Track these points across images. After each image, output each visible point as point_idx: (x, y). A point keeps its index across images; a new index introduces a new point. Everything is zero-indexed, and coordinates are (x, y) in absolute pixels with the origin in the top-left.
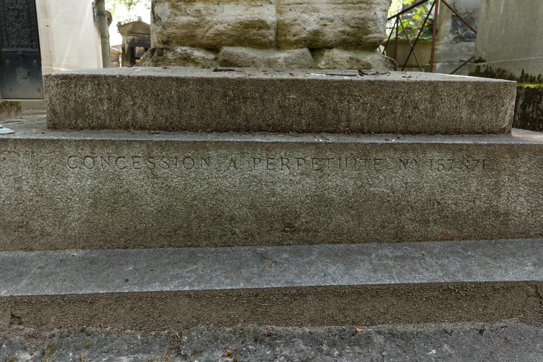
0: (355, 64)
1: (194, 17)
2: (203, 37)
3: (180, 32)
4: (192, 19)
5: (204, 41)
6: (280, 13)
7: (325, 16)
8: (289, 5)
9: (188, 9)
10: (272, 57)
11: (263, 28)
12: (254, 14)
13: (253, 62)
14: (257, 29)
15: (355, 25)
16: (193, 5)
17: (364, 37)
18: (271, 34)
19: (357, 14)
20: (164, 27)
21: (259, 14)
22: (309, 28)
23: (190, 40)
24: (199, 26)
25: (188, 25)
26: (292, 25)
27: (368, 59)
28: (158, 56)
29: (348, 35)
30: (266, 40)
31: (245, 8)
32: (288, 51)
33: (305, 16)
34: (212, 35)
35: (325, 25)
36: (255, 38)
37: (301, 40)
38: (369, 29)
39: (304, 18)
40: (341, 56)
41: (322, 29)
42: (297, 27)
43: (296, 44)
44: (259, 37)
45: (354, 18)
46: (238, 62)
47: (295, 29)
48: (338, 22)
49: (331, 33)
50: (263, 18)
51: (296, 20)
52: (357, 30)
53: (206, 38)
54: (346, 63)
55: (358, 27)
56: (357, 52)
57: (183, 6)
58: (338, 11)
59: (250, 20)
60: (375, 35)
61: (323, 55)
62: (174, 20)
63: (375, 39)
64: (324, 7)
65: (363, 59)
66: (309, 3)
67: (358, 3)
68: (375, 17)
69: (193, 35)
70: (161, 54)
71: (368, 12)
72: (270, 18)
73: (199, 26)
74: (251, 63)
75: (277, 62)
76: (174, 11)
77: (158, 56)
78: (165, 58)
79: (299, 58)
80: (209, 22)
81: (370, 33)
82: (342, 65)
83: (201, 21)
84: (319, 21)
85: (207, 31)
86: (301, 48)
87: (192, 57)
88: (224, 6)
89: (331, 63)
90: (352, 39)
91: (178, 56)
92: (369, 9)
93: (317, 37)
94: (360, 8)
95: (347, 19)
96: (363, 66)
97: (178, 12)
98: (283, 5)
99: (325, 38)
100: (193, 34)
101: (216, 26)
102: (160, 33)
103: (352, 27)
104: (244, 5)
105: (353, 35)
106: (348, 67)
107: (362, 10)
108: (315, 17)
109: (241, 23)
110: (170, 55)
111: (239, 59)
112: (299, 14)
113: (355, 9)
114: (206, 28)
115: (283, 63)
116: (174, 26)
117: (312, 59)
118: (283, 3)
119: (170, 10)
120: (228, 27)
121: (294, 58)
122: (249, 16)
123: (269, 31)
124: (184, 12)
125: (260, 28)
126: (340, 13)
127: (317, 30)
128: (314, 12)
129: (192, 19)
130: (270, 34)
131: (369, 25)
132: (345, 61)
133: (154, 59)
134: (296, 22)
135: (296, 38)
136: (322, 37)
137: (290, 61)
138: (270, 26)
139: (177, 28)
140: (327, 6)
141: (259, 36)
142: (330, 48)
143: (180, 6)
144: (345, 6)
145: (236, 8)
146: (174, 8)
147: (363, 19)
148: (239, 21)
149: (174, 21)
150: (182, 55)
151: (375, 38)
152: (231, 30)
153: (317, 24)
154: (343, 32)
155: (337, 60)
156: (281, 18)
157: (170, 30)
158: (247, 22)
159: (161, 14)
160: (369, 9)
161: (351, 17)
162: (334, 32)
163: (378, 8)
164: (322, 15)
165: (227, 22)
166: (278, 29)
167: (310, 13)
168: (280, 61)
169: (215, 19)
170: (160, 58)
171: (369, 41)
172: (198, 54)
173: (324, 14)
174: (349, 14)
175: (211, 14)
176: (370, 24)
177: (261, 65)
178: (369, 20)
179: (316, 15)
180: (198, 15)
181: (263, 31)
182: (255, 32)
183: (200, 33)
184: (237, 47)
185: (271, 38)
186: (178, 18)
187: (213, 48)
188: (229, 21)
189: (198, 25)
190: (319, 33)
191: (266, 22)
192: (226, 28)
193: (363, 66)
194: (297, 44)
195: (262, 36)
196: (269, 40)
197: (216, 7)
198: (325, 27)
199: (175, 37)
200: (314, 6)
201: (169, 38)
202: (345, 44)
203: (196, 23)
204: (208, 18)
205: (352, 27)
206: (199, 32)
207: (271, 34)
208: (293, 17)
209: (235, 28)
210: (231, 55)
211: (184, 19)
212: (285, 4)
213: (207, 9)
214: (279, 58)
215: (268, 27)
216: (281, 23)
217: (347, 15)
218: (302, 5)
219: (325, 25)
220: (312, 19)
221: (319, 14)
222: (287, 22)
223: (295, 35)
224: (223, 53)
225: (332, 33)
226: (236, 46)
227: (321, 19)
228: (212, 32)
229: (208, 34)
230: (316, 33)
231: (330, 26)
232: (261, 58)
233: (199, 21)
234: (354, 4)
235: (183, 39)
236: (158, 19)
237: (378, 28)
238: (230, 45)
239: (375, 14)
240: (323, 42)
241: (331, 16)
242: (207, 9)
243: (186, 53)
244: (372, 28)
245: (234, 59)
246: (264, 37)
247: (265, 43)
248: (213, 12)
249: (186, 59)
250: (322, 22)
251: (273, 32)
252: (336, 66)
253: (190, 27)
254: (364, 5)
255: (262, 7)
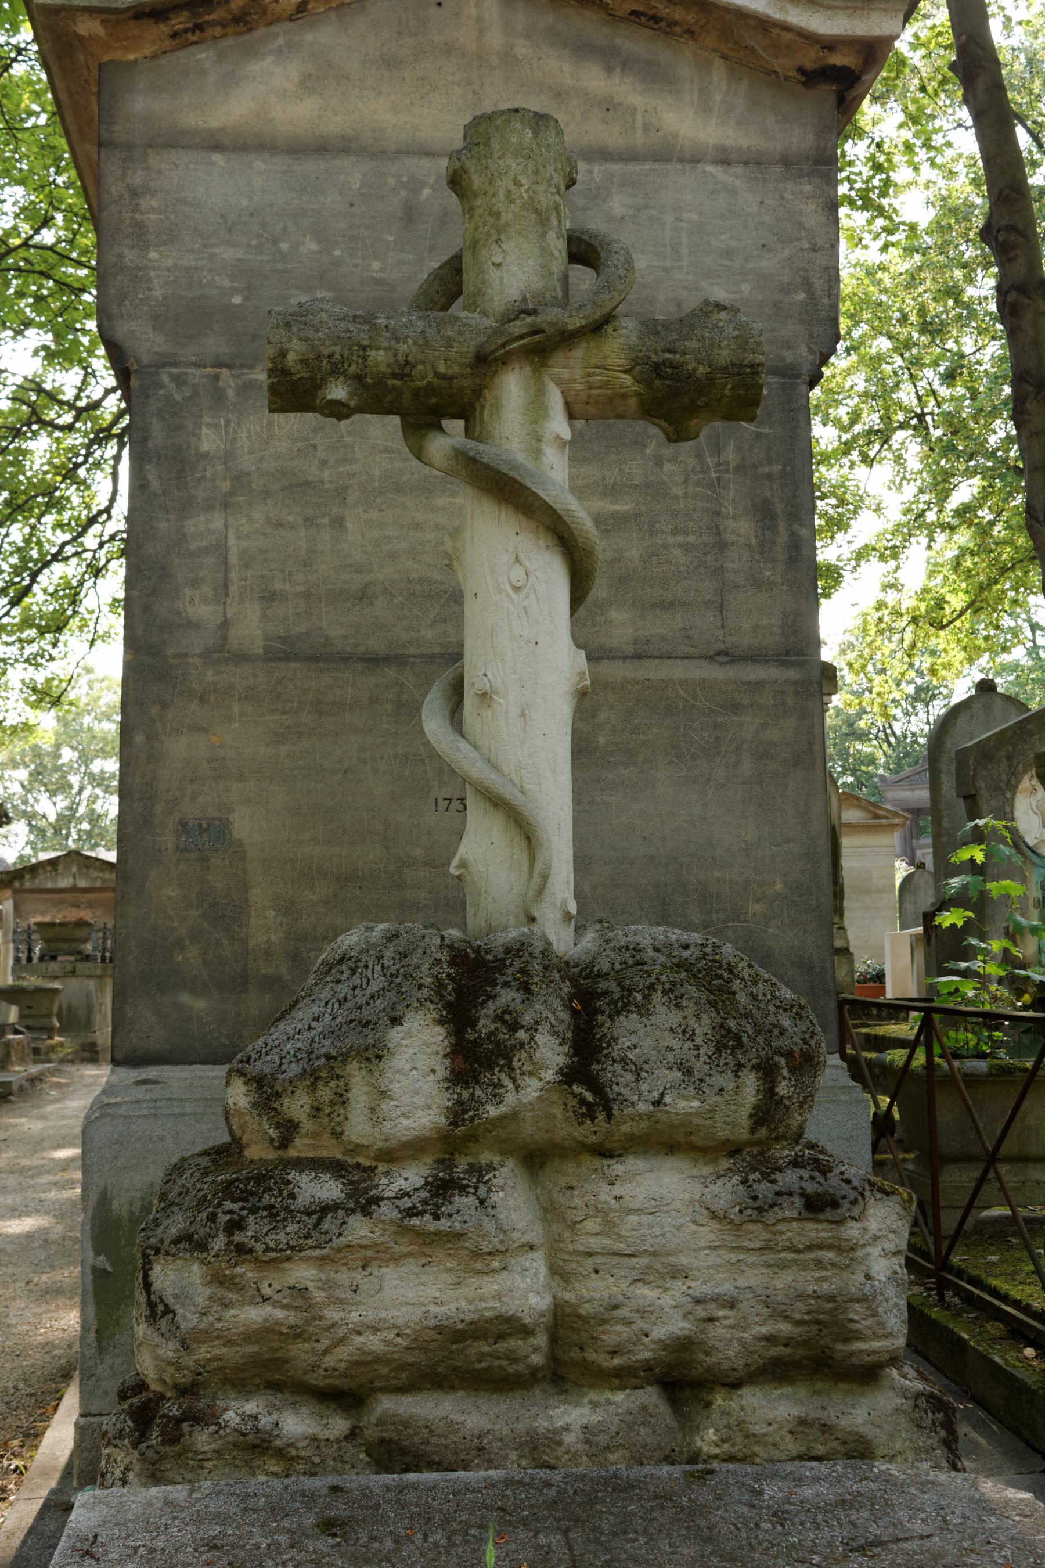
0: (815, 1441)
1: (285, 1307)
2: (314, 1367)
3: (233, 1355)
4: (279, 1314)
5: (317, 1379)
6: (562, 1276)
7: (708, 1290)
8: (590, 1255)
9: (266, 1284)
10: (542, 1424)
11: (511, 1335)
12: (481, 1300)
13: (480, 1449)
14: (492, 1341)
15: (806, 1317)
16: (283, 1270)
17: (839, 1347)
18: (536, 1349)
19: (808, 1281)
20: (185, 1345)
21: (498, 1297)
22: (659, 1333)
23: (270, 1372)
24: (299, 1335)
25: (267, 1331)
26: (603, 1322)
27: (860, 1420)
28: (164, 1443)
29: (786, 1345)
30: (520, 1367)
31: (450, 1279)
32: (593, 1395)
33: (647, 1294)
34: (343, 1364)
35: (711, 1320)
36: (483, 1365)
37: (637, 1369)
38: (857, 1326)
39: (641, 1302)
40: (771, 1414)
41: (702, 1332)
42: (619, 1328)
43: (618, 1376)
44: (497, 1363)
45: (801, 1296)
46: (429, 1448)
47: (615, 1334)
48: (749, 1307)
49: (729, 1343)
50: (511, 1307)
51: (616, 1307)
52: (814, 1328)
53: (321, 1372)
54: (788, 1438)
55: (818, 1322)
56: (819, 1386)
57: (250, 1275)
58: (749, 1272)
59: (468, 1318)
60: (876, 1344)
61: (708, 1405)
62: (219, 1320)
63: (875, 1358)
64: (705, 1259)
65: (843, 1422)
66: (654, 1254)
67: (810, 1248)
68: (867, 1290)
69: (277, 1359)
70: (172, 1438)
71: (846, 1275)
72: (534, 1300)
73: (299, 1335)
74: (474, 1453)
75: (560, 1443)
76: (221, 1292)
77: (164, 1443)
78: (187, 1449)
79: (630, 1426)
80: (333, 1325)
81: (857, 1339)
82: (774, 1445)
83: (308, 1323)
84: (689, 1306)
85: (325, 1352)
86: (636, 1388)
87: (278, 1443)
88: (385, 1270)
89: (739, 1439)
90: (800, 1352)
91: (230, 1439)
92: (848, 1266)
93: (686, 1356)
94: (819, 1264)
95: (779, 1298)
96: (845, 1443)
97: (233, 1296)
98: (570, 1254)
99: (714, 1359)
100: (279, 1354)
101: (359, 1339)
102: (170, 1363)
103: (799, 1323)
104: (448, 1270)
105: (805, 1343)
106: (794, 1449)
107: (826, 1269)
108: (677, 1294)
109: (439, 1329)
110: (202, 1439)
111: (434, 1440)
112: (624, 1286)
113: (803, 1266)
114: (325, 1343)
115: (580, 1447)
116: (218, 1338)
117: (674, 1424)
118: (571, 1248)
119: (208, 1292)
120: (399, 1340)
121: (614, 1429)
122: (464, 1305)
123: (531, 1341)
124: (252, 1292)
125: (501, 1337)
126: (754, 1278)
127: (686, 1337)
128: (674, 1278)
129: (279, 1314)
130: (535, 1352)
131: (852, 1316)
132: (784, 1432)
133: (150, 1454)
134: (615, 1313)
135: (617, 1361)
136: (702, 1356)
137: (602, 1439)
138: (531, 1326)
139: (229, 1343)
140: (713, 1259)
141: (499, 1358)
142: (736, 1385)
143: (241, 1276)
144: (771, 1258)
145: (424, 1278)
146: (221, 1283)
147: (831, 1298)
148: (432, 1323)
149: (218, 1325)
150: (244, 1435)
151: (874, 1352)
152: (407, 1349)
153: (685, 1316)
154: (771, 1339)
155: (758, 1429)
156: (567, 1296)
157: (204, 1352)
158: (460, 1326)
159: (176, 1296)
160: (848, 1266)
161: (792, 1294)
162: (740, 1340)
163: (875, 1251)
164: (698, 1287)
165: (395, 1326)
166: (556, 1325)
167: (659, 1282)
168: (569, 1439)
169: (354, 1316)
170: (168, 1449)
171: (854, 1360)
172: (295, 1424)
173: (705, 1282)
174: (784, 1281)
175: (342, 1301)
176: (856, 1311)
177: (505, 1458)
178: (851, 1300)
179: (680, 1286)
180: (299, 1302)
181: (513, 1343)
182: (486, 1349)
183: (303, 1356)
184: (425, 1394)
185: (536, 1359)
186: (232, 1312)
187: (344, 1396)
188: (400, 1322)
189: (297, 1334)
190: (693, 1343)
191: (518, 1319)
192: (388, 1343)
193: (845, 1443)
194: (624, 1377)
195: (507, 1358)
196: (529, 1366)
197: (358, 1276)
198: (710, 1327)
199: (220, 1369)
200: (673, 1259)
201: (199, 1374)
202: (776, 1370)
203: (291, 1327)
204: (333, 1314)
205: (799, 1323)
206: (300, 1352)
207: (536, 1349)
208: (605, 1294)
209: (418, 1344)
210: (406, 1424)
211: (254, 1315)
212: (576, 1252)
213: (328, 1285)
214: (567, 1428)
215: (526, 1332)
216: (568, 1311)
217: (779, 1284)
218: (634, 1260)
219: (711, 1320)
220: (667, 1300)
221: (689, 1283)
222: (586, 1309)
223: (613, 1353)
224: (380, 1419)
225: (735, 1344)
226: (420, 1389)
227: (698, 1301)
228: (346, 1357)
229: (329, 1361)
230: (683, 1345)
231: (727, 1322)
232: (506, 1431)
233: (300, 1323)
234: (799, 1252)
235: (243, 1371)
236: (164, 1314)
237: (882, 1324)
238: (403, 1389)
239: (868, 1277)
240: (708, 1369)
241: (726, 1288)
242: (328, 1285)
243: (258, 1431)
244: (865, 1324)
245: (416, 1439)
246: (515, 1360)
247: (518, 1376)
248: (349, 1294)
249: (254, 1447)
250: (700, 1312)
251: (541, 1340)
252: (756, 1449)
253: (271, 1336)
254: (830, 1255)
255: (505, 1273)
